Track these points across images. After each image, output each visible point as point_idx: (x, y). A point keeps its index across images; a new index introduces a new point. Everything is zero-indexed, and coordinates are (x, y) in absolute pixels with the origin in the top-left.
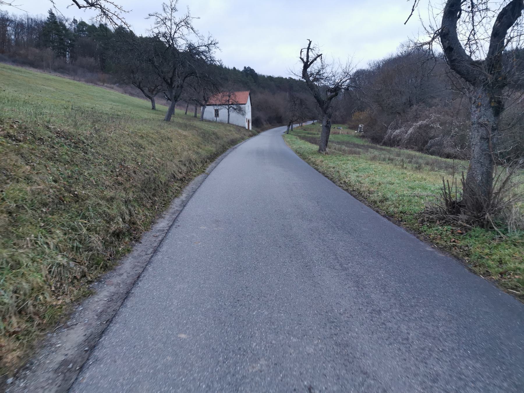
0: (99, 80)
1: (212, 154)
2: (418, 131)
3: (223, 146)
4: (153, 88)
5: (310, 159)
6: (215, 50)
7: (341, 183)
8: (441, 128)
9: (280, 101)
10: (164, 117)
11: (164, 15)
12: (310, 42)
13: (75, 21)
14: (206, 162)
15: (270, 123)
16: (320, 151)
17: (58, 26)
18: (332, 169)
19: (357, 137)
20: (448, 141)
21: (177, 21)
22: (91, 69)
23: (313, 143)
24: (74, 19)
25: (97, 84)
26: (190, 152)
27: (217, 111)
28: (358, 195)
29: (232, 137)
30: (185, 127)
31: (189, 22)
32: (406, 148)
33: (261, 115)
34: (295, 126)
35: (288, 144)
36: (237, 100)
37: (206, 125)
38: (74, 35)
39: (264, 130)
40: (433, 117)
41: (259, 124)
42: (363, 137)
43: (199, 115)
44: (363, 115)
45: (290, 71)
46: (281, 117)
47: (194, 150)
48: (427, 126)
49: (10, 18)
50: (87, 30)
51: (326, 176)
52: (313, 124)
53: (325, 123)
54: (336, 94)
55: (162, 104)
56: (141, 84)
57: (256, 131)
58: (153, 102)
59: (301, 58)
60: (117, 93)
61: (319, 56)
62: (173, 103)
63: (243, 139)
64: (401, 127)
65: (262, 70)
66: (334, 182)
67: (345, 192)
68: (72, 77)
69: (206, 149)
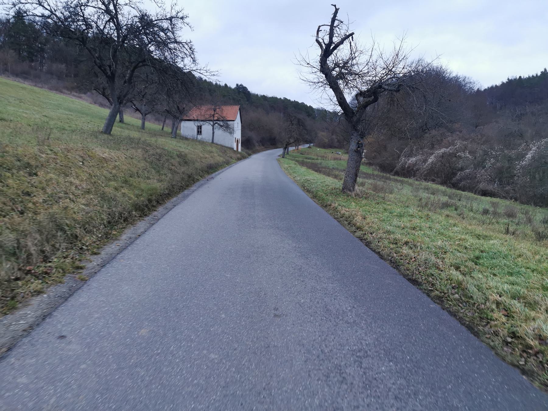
3: (189, 177)
5: (335, 209)
9: (275, 122)
12: (337, 10)
16: (347, 189)
18: (405, 250)
20: (481, 173)
22: (60, 77)
25: (61, 92)
27: (199, 128)
29: (212, 161)
33: (253, 135)
34: (291, 149)
36: (224, 115)
39: (255, 152)
40: (459, 144)
41: (249, 145)
46: (274, 139)
48: (453, 155)
52: (309, 147)
53: (353, 146)
54: (376, 100)
55: (137, 118)
57: (246, 153)
59: (317, 41)
61: (347, 37)
63: (228, 163)
65: (255, 89)
68: (34, 84)
69: (143, 186)
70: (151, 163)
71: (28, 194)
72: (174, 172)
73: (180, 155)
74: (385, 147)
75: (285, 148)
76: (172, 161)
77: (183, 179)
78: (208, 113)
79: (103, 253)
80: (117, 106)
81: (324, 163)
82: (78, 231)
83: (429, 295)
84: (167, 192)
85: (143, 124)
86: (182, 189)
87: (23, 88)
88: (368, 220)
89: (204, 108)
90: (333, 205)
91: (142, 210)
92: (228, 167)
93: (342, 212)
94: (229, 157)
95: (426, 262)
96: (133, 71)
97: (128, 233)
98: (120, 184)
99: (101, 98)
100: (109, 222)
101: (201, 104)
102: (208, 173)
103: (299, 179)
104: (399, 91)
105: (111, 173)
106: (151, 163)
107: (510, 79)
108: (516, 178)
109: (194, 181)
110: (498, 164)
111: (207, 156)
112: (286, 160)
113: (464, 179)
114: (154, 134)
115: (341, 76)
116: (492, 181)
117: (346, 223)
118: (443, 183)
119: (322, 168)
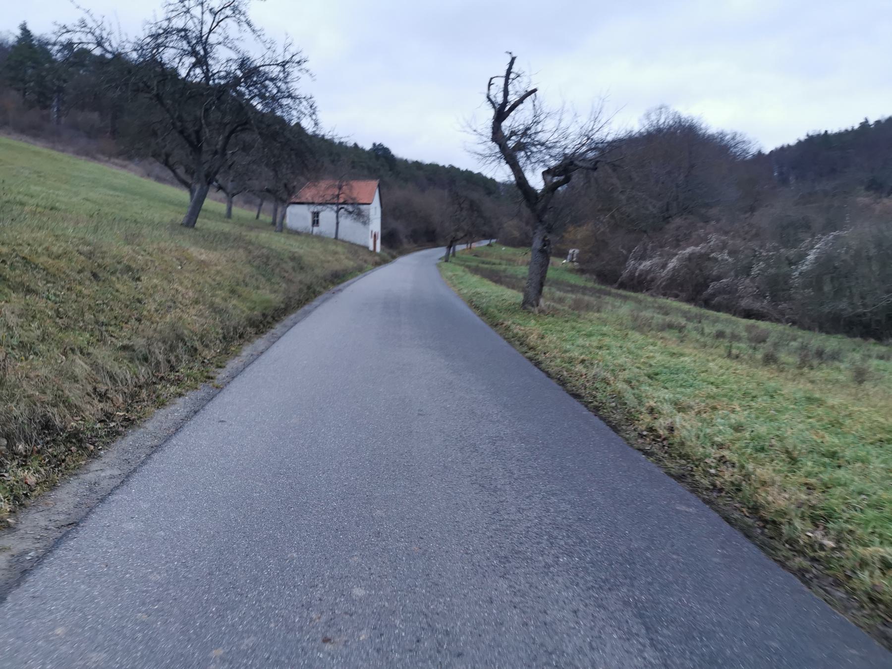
0: (103, 153)
2: (686, 266)
3: (309, 288)
5: (508, 328)
6: (299, 74)
7: (641, 436)
8: (730, 260)
9: (434, 204)
12: (513, 59)
15: (415, 241)
16: (529, 304)
18: (579, 368)
19: (571, 271)
20: (745, 284)
22: (92, 133)
27: (316, 215)
29: (337, 267)
32: (664, 295)
33: (400, 226)
34: (459, 248)
36: (355, 195)
37: (283, 240)
39: (403, 253)
40: (714, 239)
41: (393, 242)
42: (582, 271)
43: (278, 220)
44: (582, 232)
46: (434, 232)
48: (706, 256)
51: (577, 396)
52: (489, 245)
53: (537, 243)
55: (215, 200)
56: (170, 159)
57: (389, 254)
59: (489, 99)
63: (360, 270)
65: (402, 151)
66: (615, 429)
67: (681, 489)
69: (254, 296)
70: (258, 268)
71: (139, 301)
72: (290, 281)
73: (293, 258)
75: (449, 247)
76: (284, 265)
77: (300, 290)
78: (330, 192)
79: (227, 366)
80: (205, 188)
81: (511, 270)
82: (197, 344)
83: (586, 406)
84: (283, 306)
85: (230, 209)
86: (301, 303)
88: (547, 340)
89: (323, 184)
90: (506, 323)
91: (258, 327)
92: (361, 275)
93: (515, 331)
94: (363, 261)
95: (595, 377)
96: (228, 137)
97: (247, 351)
98: (228, 294)
99: (158, 168)
100: (224, 338)
101: (317, 179)
102: (334, 283)
103: (465, 291)
104: (596, 169)
105: (214, 280)
106: (258, 268)
107: (811, 134)
108: (793, 291)
109: (316, 294)
110: (772, 271)
111: (330, 258)
113: (720, 293)
114: (241, 222)
115: (520, 147)
116: (760, 296)
117: (517, 343)
118: (689, 300)
119: (506, 277)
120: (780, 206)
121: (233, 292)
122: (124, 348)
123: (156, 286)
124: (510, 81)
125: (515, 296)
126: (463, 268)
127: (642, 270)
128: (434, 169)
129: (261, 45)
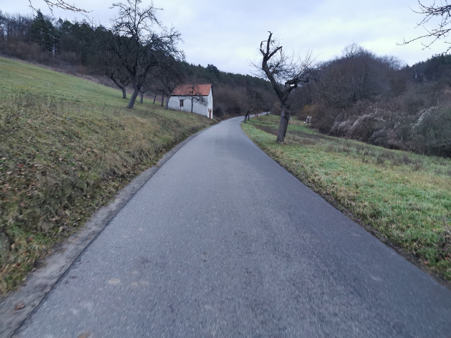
0: (79, 72)
1: (169, 143)
2: (363, 124)
3: (183, 134)
4: (124, 79)
5: (269, 150)
6: (178, 41)
7: (309, 182)
8: (384, 121)
9: (239, 94)
10: (128, 104)
11: (129, 6)
12: (271, 34)
13: (60, 20)
14: (161, 151)
15: (230, 114)
16: (279, 141)
17: (45, 24)
18: (294, 163)
19: (307, 127)
20: (390, 132)
21: (141, 12)
22: (73, 62)
23: (268, 132)
24: (60, 19)
25: (76, 75)
26: (143, 141)
27: (182, 101)
28: (335, 201)
30: (145, 114)
31: (153, 13)
32: (352, 138)
33: (222, 106)
34: (251, 116)
35: (245, 132)
36: (200, 92)
37: (169, 113)
38: (59, 33)
39: (224, 119)
40: (376, 111)
41: (219, 114)
42: (312, 127)
43: (164, 104)
44: (312, 108)
45: (250, 63)
46: (239, 108)
47: (149, 139)
48: (371, 119)
49: (3, 16)
50: (71, 28)
51: (290, 172)
52: (267, 115)
53: (283, 114)
56: (113, 76)
58: (124, 91)
59: (261, 50)
60: (93, 83)
61: (278, 48)
62: (135, 91)
63: (204, 127)
64: (346, 120)
65: (222, 68)
66: (301, 181)
67: (317, 195)
68: (55, 69)
69: (163, 137)
72: (175, 131)
74: (151, 113)
77: (180, 135)
78: (189, 90)
86: (181, 140)
87: (50, 73)
89: (185, 87)
97: (165, 156)
99: (105, 79)
100: (156, 151)
107: (434, 56)
111: (190, 122)
112: (247, 125)
114: (148, 105)
118: (364, 141)
119: (274, 130)
120: (412, 93)
121: (155, 135)
122: (127, 152)
123: (130, 132)
124: (270, 43)
125: (273, 137)
126: (252, 126)
127: (341, 126)
128: (239, 77)
129: (161, 29)
